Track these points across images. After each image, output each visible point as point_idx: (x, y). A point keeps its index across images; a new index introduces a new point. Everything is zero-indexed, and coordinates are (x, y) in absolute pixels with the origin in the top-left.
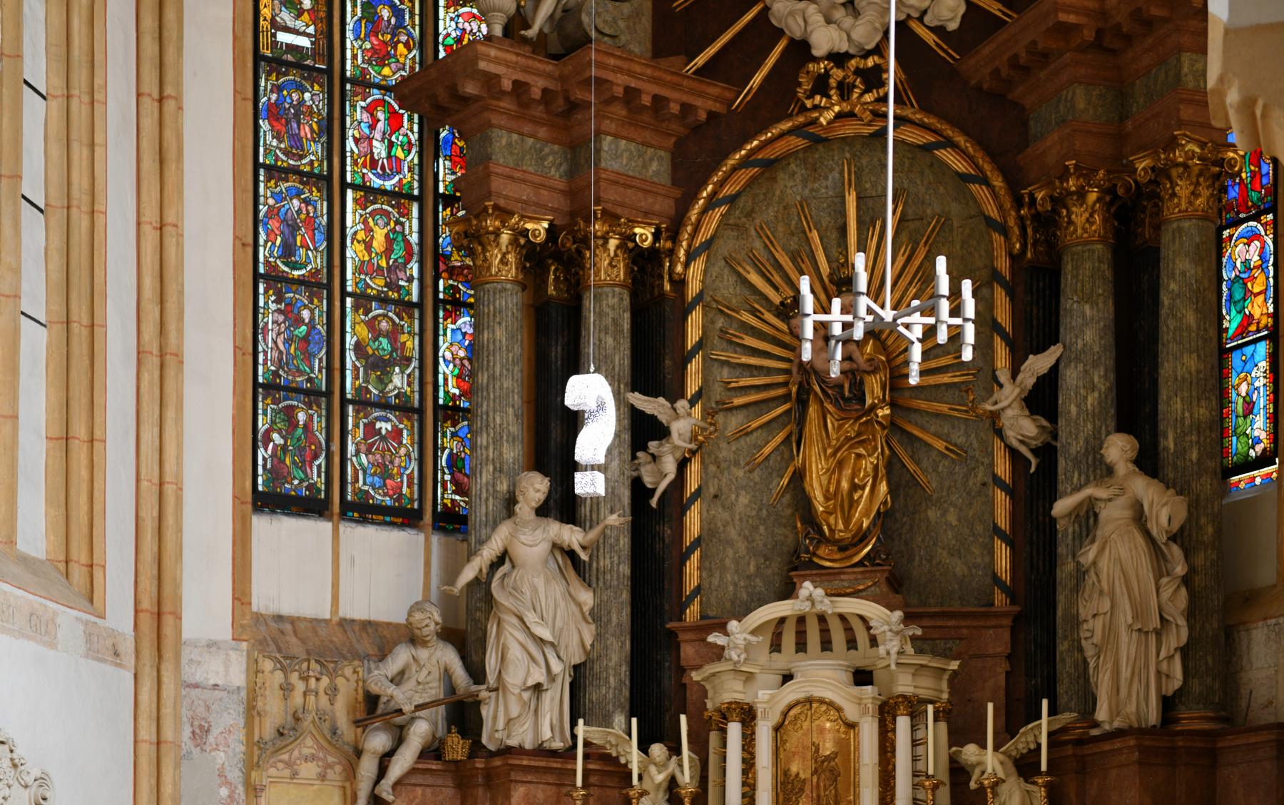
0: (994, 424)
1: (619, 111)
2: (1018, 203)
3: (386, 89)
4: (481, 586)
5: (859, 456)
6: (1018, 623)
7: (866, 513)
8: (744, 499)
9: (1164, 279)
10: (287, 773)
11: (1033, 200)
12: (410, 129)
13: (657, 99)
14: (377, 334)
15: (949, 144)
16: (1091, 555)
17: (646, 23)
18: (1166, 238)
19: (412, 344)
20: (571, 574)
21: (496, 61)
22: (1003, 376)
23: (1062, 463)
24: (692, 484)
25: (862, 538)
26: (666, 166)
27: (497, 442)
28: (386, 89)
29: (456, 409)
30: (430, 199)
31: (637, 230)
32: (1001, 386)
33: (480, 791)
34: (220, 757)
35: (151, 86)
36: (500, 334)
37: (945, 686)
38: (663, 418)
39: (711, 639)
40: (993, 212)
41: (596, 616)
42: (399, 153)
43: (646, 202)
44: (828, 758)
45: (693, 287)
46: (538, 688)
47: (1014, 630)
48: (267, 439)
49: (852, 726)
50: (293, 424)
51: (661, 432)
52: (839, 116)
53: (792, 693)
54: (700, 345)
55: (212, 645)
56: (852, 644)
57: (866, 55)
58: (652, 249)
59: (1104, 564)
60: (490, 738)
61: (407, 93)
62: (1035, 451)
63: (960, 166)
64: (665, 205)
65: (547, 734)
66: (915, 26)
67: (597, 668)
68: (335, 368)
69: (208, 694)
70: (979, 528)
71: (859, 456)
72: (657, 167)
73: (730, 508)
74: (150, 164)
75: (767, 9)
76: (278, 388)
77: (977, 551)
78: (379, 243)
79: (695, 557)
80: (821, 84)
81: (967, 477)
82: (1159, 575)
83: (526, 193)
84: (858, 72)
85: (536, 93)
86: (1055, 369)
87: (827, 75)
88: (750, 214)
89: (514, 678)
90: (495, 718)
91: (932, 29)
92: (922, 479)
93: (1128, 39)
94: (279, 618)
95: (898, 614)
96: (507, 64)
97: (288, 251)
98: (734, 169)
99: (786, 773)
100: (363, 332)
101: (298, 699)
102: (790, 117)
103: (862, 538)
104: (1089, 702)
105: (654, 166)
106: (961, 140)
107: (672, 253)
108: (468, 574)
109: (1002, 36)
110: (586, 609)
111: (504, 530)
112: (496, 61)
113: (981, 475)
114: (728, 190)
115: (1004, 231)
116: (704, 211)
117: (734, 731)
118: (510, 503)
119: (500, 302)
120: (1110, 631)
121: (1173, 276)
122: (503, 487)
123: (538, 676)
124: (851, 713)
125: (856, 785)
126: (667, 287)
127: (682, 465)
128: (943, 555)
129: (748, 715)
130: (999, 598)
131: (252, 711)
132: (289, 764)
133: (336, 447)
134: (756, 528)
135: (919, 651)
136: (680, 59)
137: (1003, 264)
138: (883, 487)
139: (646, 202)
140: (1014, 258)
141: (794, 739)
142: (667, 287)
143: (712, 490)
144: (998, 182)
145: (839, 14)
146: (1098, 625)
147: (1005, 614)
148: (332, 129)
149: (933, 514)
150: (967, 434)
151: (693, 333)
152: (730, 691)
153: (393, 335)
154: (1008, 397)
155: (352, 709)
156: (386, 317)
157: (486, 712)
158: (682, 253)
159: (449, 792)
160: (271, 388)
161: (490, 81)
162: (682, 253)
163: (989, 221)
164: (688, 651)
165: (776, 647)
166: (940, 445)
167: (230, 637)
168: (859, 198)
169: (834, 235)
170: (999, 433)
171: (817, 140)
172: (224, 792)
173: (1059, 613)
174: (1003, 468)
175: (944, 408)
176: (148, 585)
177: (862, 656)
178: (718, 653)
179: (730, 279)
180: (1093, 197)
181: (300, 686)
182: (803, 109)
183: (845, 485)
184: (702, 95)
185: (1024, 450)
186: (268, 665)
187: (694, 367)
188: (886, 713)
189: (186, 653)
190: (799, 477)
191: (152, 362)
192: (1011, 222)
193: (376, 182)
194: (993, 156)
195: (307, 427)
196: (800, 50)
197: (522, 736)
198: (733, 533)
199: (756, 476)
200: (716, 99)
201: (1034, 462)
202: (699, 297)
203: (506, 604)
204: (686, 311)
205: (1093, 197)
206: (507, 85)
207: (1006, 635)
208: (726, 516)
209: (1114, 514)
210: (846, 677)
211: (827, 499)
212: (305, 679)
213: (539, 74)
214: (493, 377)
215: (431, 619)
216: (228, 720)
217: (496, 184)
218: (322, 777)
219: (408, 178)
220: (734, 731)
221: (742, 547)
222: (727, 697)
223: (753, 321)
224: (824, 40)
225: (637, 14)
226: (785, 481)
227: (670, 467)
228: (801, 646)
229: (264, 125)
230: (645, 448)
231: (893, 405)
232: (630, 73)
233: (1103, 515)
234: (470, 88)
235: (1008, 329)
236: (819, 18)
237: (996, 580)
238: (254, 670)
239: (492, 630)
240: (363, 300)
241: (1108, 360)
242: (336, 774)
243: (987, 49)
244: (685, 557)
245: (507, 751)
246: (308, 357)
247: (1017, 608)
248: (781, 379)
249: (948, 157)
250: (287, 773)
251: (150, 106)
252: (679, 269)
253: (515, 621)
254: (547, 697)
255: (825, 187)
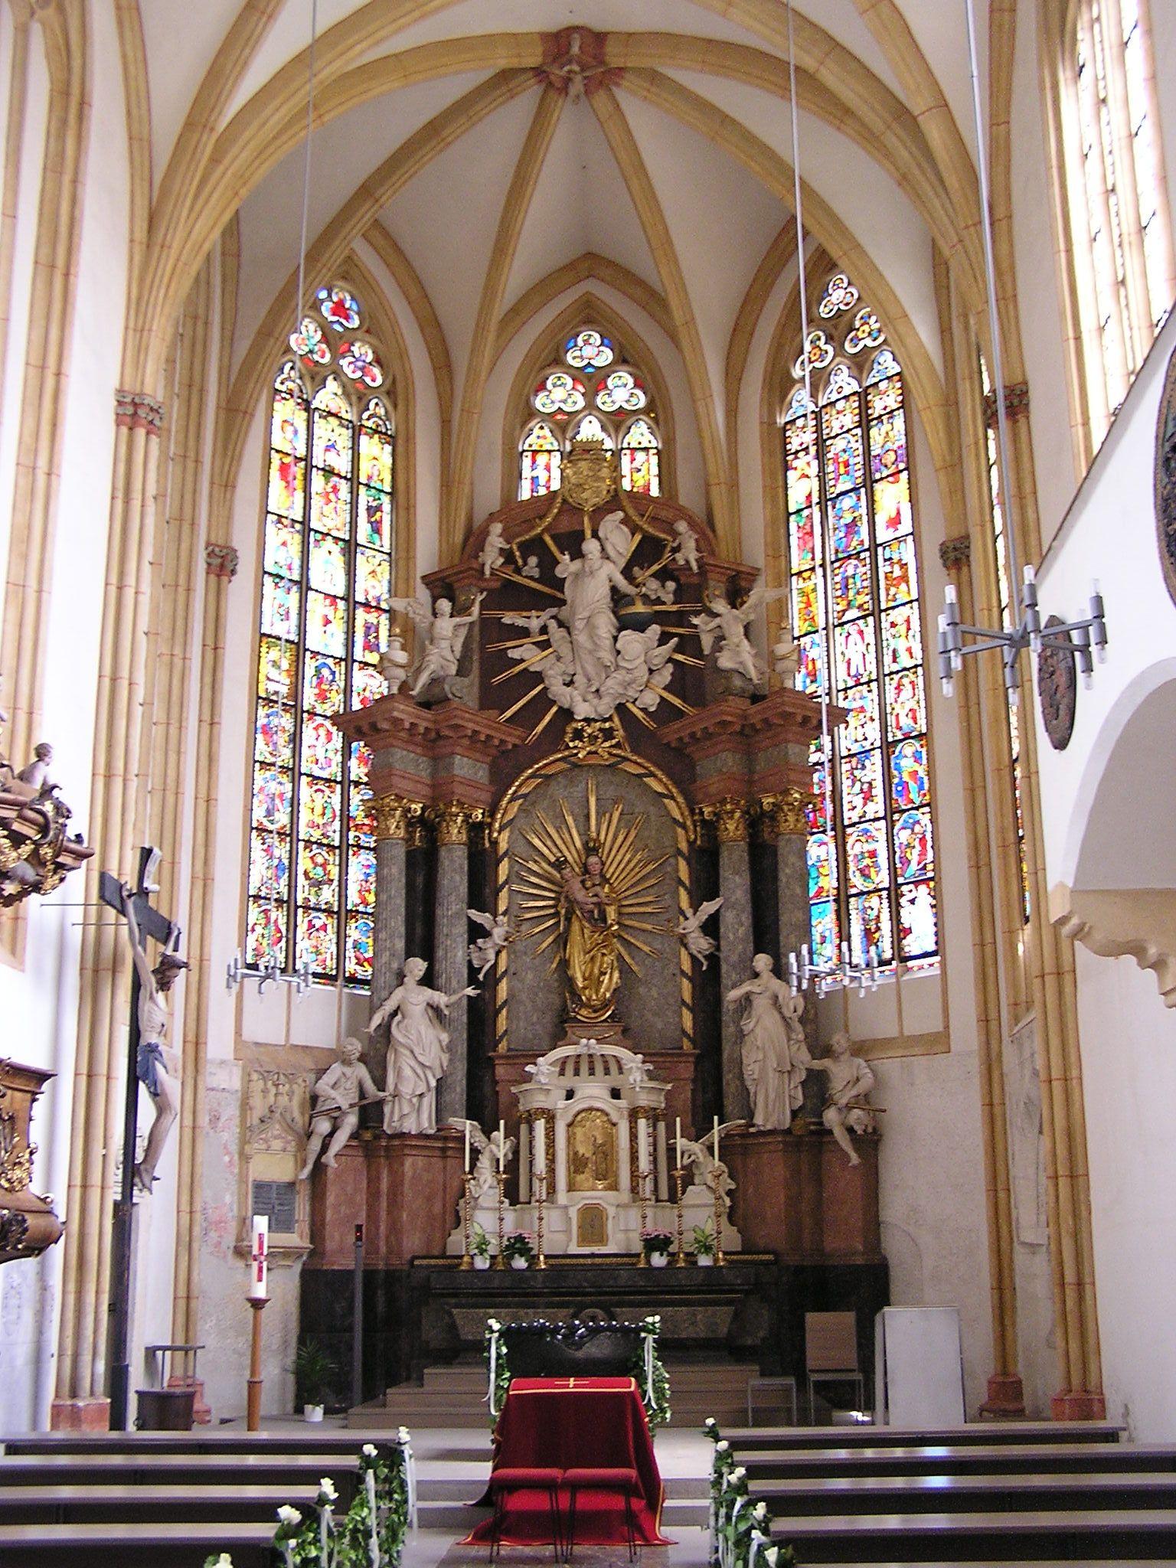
0: (682, 940)
1: (466, 742)
2: (692, 812)
3: (326, 717)
4: (385, 1029)
5: (604, 955)
6: (699, 1060)
7: (607, 990)
8: (530, 976)
9: (781, 865)
10: (264, 1146)
11: (702, 813)
12: (338, 741)
13: (488, 736)
14: (316, 865)
15: (652, 775)
16: (751, 1025)
17: (476, 690)
18: (781, 844)
19: (334, 872)
20: (436, 1021)
21: (402, 711)
22: (689, 912)
23: (724, 968)
24: (502, 968)
25: (605, 1005)
26: (487, 773)
27: (391, 937)
28: (326, 717)
29: (357, 911)
30: (346, 783)
31: (413, 806)
32: (687, 919)
33: (382, 1160)
34: (225, 1136)
35: (206, 717)
36: (395, 870)
37: (662, 1098)
38: (487, 926)
39: (527, 1069)
40: (679, 817)
41: (450, 1049)
42: (330, 754)
43: (477, 794)
44: (601, 1145)
45: (503, 846)
46: (421, 1095)
47: (696, 1064)
48: (253, 930)
49: (614, 1125)
50: (268, 919)
51: (486, 934)
52: (589, 753)
53: (577, 1105)
54: (506, 882)
55: (223, 1062)
56: (607, 1072)
57: (605, 720)
58: (481, 823)
59: (758, 1030)
60: (389, 1125)
61: (335, 719)
62: (705, 957)
63: (660, 789)
64: (486, 796)
65: (426, 1125)
66: (630, 706)
67: (449, 1081)
68: (292, 886)
69: (219, 1095)
70: (672, 1001)
71: (604, 955)
72: (482, 774)
73: (522, 981)
74: (204, 762)
75: (545, 689)
76: (260, 897)
77: (669, 1014)
78: (318, 810)
79: (504, 1012)
80: (578, 735)
81: (663, 969)
82: (789, 1039)
83: (410, 786)
84: (600, 730)
85: (422, 730)
86: (718, 911)
87: (582, 730)
88: (533, 804)
89: (406, 1089)
90: (392, 1113)
91: (642, 710)
92: (635, 968)
93: (757, 731)
94: (257, 1044)
95: (640, 1056)
96: (409, 714)
97: (269, 813)
98: (528, 778)
99: (576, 1153)
100: (309, 865)
101: (271, 1099)
102: (559, 751)
103: (605, 1005)
104: (751, 1115)
105: (481, 773)
106: (659, 773)
107: (490, 825)
108: (377, 1020)
109: (685, 721)
110: (444, 1044)
111: (399, 993)
112: (402, 711)
113: (672, 969)
114: (524, 790)
115: (684, 826)
116: (510, 802)
117: (540, 1125)
118: (401, 978)
119: (395, 852)
120: (763, 1070)
121: (786, 865)
122: (395, 965)
123: (422, 1089)
124: (614, 1118)
125: (618, 1161)
126: (487, 845)
127: (498, 953)
128: (649, 1016)
129: (550, 1117)
130: (687, 1045)
131: (245, 1105)
132: (266, 1141)
133: (291, 936)
134: (536, 994)
135: (651, 1079)
136: (496, 712)
137: (683, 846)
138: (616, 975)
139: (477, 794)
140: (691, 844)
141: (579, 1131)
142: (487, 845)
143: (512, 970)
144: (680, 799)
145: (590, 697)
146: (756, 1067)
147: (691, 1055)
148: (296, 739)
149: (642, 990)
150: (663, 944)
151: (502, 879)
152: (539, 1101)
153: (324, 866)
154: (692, 924)
155: (302, 1105)
156: (322, 856)
157: (387, 1109)
158: (497, 825)
159: (361, 1159)
160: (257, 897)
161: (396, 722)
162: (497, 825)
163: (675, 821)
164: (501, 1071)
165: (562, 1073)
166: (646, 949)
167: (232, 1057)
168: (597, 799)
169: (582, 819)
170: (685, 946)
171: (575, 766)
172: (227, 1159)
173: (725, 1055)
174: (686, 966)
175: (649, 927)
176: (192, 1025)
177: (615, 1079)
178: (528, 1078)
179: (522, 842)
180: (737, 815)
181: (273, 1090)
182: (568, 747)
183: (596, 971)
184: (510, 735)
185: (700, 956)
186: (255, 1076)
187: (504, 894)
188: (634, 1114)
189: (210, 1068)
190: (565, 964)
191: (199, 884)
192: (689, 823)
193: (317, 773)
194: (677, 784)
195: (276, 921)
196: (566, 714)
197: (410, 1126)
198: (524, 997)
199: (537, 961)
200: (519, 737)
201: (705, 963)
202: (506, 854)
203: (401, 1039)
204: (499, 861)
205: (737, 815)
206: (407, 725)
207: (692, 1068)
208: (520, 985)
209: (761, 1004)
210: (606, 1095)
211: (585, 979)
212: (277, 1085)
213: (425, 719)
214: (390, 897)
215: (355, 1047)
216: (230, 1112)
217: (395, 780)
218: (284, 1150)
219: (334, 771)
220: (540, 1125)
221: (529, 1005)
222: (537, 1105)
223: (535, 868)
224: (582, 710)
225: (472, 685)
226: (554, 966)
227: (492, 956)
228: (577, 1073)
229: (260, 736)
230: (475, 943)
231: (618, 923)
232: (477, 723)
233: (755, 1003)
234: (385, 725)
235: (687, 882)
236: (580, 698)
237: (684, 1032)
238: (247, 1080)
239: (391, 1057)
240: (309, 843)
241: (749, 908)
242: (292, 1147)
243: (677, 725)
244: (498, 1012)
245: (402, 1135)
246: (278, 878)
247: (697, 1051)
248: (551, 903)
249: (650, 781)
250: (264, 1146)
251: (206, 727)
252: (495, 835)
253: (407, 1053)
254: (426, 1101)
255: (577, 791)
